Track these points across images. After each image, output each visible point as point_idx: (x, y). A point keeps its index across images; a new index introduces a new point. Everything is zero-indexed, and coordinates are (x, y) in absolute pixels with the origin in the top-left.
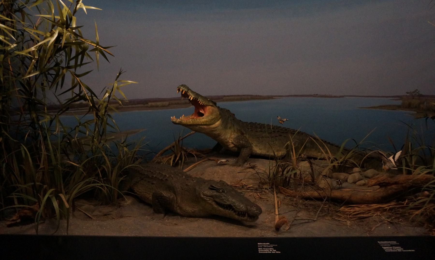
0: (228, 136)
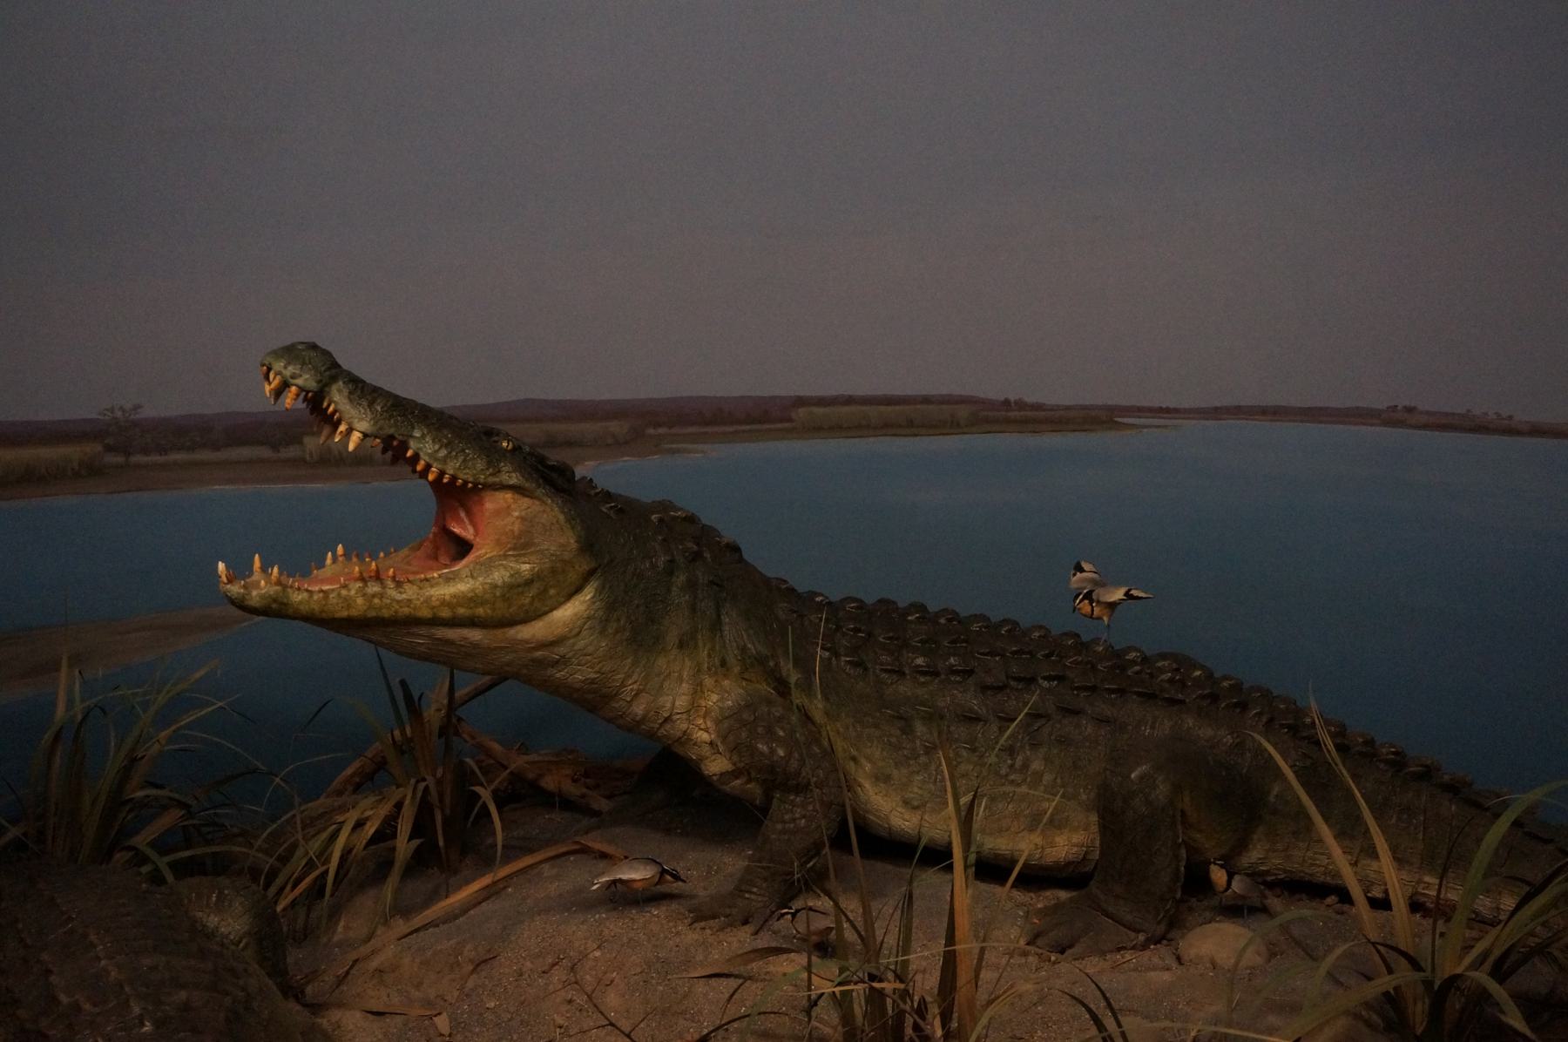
0: (676, 698)
